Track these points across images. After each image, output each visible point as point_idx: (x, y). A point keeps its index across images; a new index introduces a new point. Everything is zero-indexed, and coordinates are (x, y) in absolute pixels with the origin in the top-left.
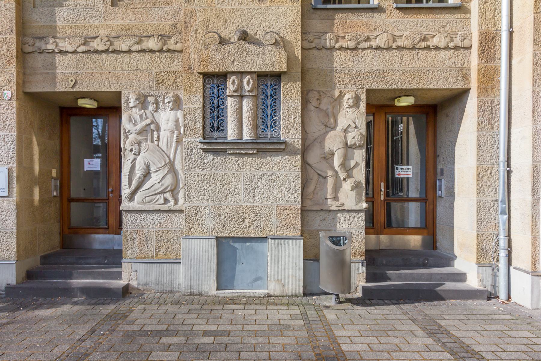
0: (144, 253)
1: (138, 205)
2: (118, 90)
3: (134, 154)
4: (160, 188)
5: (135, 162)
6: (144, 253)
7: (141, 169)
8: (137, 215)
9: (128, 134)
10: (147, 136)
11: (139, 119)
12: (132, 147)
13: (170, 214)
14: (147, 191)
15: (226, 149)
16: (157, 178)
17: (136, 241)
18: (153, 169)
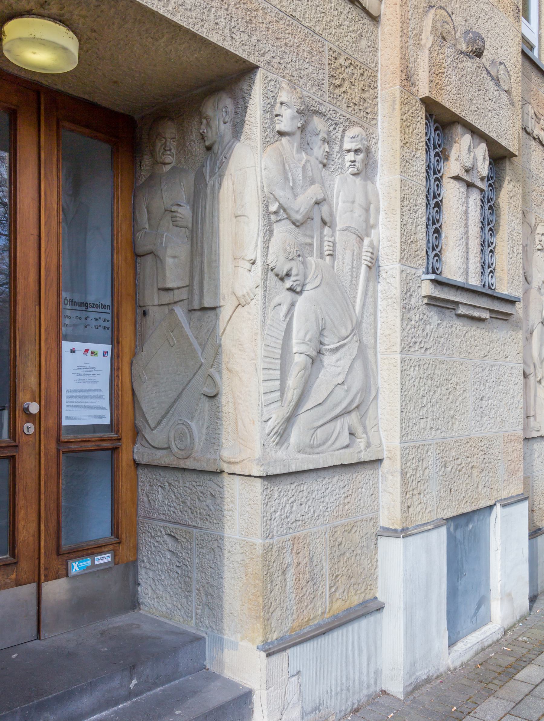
0: (307, 606)
1: (300, 456)
2: (251, 59)
3: (290, 289)
4: (344, 398)
5: (293, 314)
6: (307, 606)
7: (310, 340)
8: (293, 486)
9: (273, 218)
10: (312, 237)
11: (301, 178)
12: (293, 264)
13: (354, 476)
14: (320, 408)
15: (457, 303)
16: (339, 369)
17: (290, 574)
18: (330, 342)
